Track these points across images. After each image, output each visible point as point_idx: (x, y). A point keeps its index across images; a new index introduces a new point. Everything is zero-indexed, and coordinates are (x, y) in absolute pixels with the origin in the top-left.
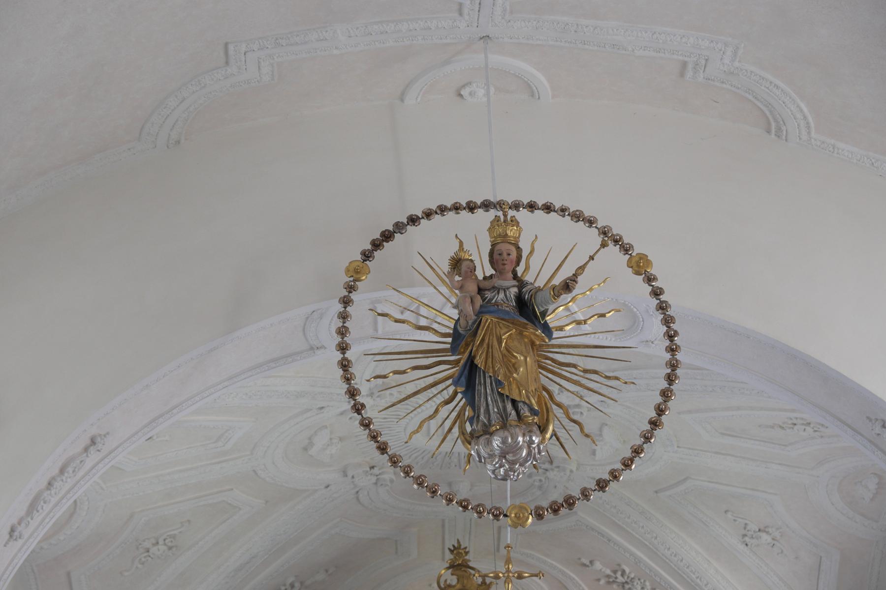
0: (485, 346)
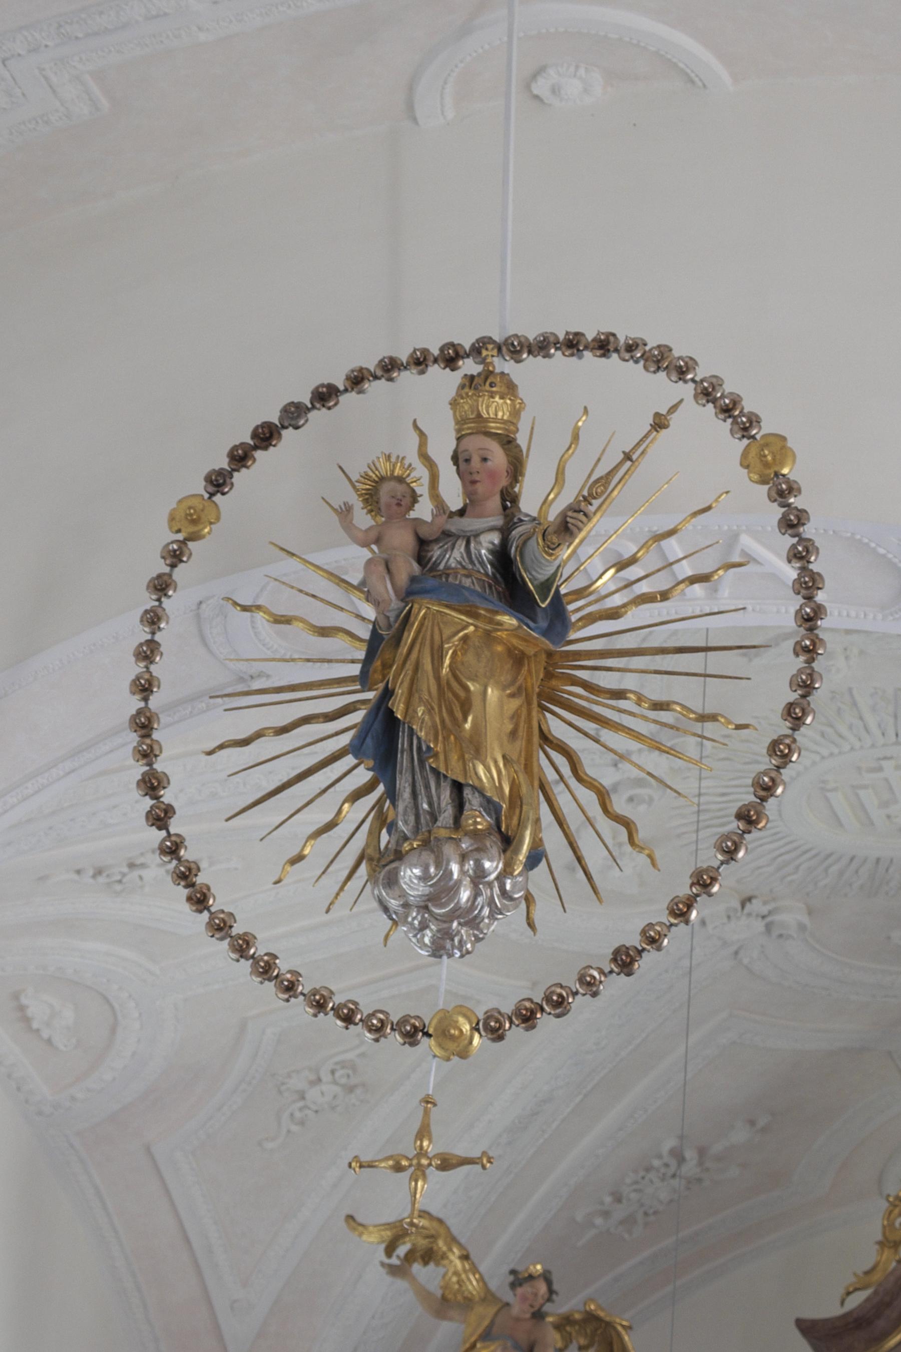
0: (409, 666)
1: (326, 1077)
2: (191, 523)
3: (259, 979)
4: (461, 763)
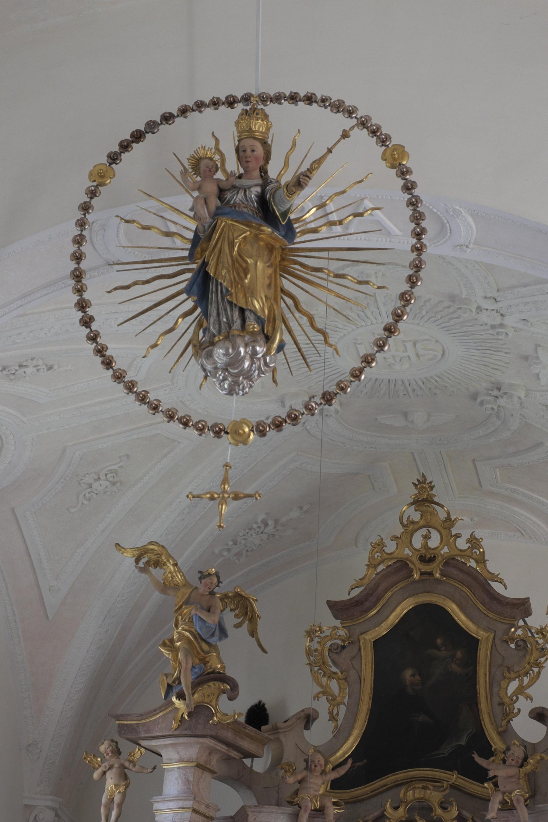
0: (217, 250)
1: (103, 477)
2: (99, 179)
3: (139, 403)
4: (244, 298)
